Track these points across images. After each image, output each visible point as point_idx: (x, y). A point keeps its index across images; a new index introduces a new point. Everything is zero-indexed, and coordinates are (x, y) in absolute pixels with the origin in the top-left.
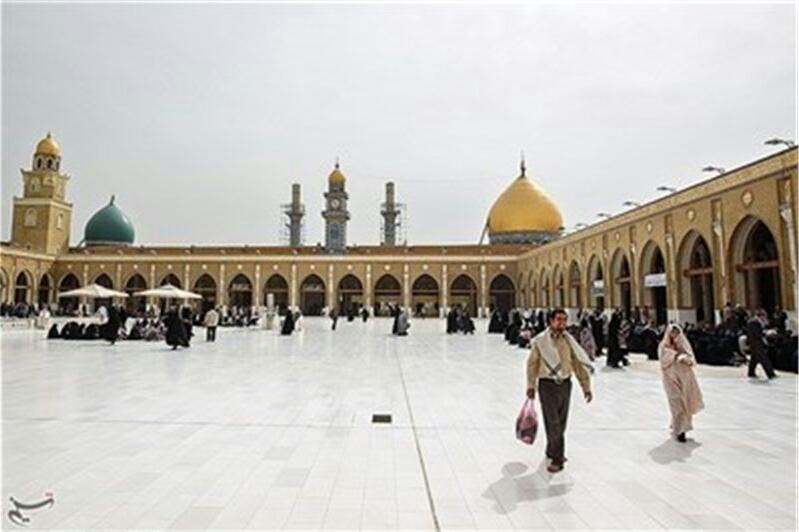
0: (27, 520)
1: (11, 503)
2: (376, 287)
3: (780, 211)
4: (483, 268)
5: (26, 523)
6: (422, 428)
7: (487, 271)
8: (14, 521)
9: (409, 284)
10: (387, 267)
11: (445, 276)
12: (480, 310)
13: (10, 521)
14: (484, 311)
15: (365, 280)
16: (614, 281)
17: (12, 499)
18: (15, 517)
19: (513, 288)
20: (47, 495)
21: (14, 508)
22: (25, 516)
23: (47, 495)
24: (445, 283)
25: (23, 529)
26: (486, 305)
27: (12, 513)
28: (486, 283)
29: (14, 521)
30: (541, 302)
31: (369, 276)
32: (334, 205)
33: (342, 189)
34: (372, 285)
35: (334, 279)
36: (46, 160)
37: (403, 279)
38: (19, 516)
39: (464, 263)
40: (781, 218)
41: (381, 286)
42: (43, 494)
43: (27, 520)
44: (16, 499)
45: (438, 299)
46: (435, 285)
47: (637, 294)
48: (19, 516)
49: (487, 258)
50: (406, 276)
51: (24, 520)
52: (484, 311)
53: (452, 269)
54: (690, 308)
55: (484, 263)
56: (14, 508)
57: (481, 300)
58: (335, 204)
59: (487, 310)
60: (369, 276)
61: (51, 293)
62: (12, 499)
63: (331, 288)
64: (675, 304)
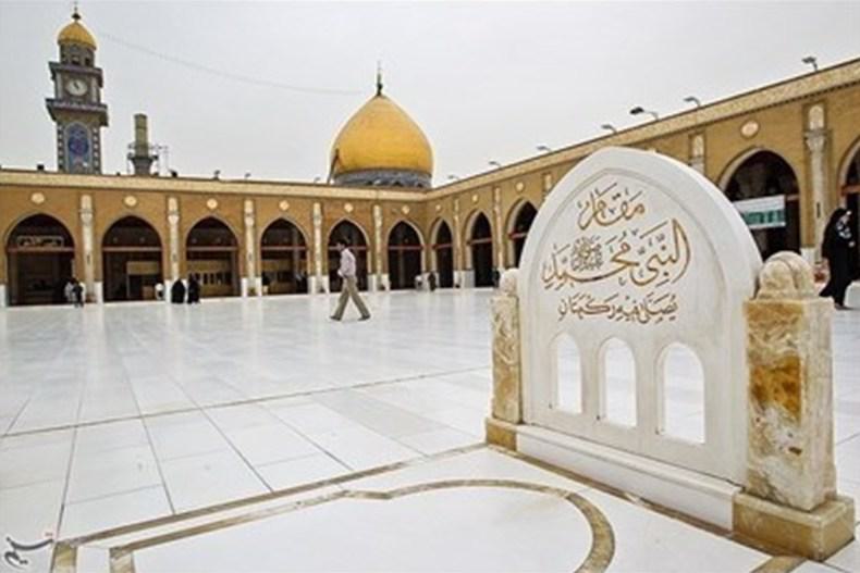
0: (26, 562)
1: (8, 544)
2: (189, 243)
3: (806, 139)
4: (377, 210)
5: (24, 566)
6: (259, 466)
7: (383, 214)
8: (10, 563)
9: (255, 235)
10: (212, 204)
11: (318, 223)
12: (244, 282)
13: (6, 563)
14: (379, 279)
15: (167, 229)
16: (507, 236)
17: (8, 539)
18: (12, 559)
19: (417, 242)
20: (47, 534)
21: (11, 549)
22: (22, 558)
23: (47, 534)
24: (318, 233)
25: (15, 570)
26: (324, 274)
27: (8, 555)
28: (383, 234)
29: (10, 563)
30: (464, 263)
31: (173, 219)
32: (72, 89)
33: (89, 62)
34: (180, 237)
35: (95, 224)
36: (76, 62)
37: (243, 226)
38: (16, 557)
39: (349, 200)
40: (806, 147)
41: (194, 241)
42: (43, 534)
43: (26, 562)
44: (13, 539)
45: (230, 264)
46: (230, 239)
47: (460, 257)
48: (16, 557)
49: (385, 194)
50: (249, 222)
51: (22, 562)
52: (379, 279)
53: (329, 208)
54: (470, 270)
55: (378, 202)
56: (11, 549)
57: (245, 263)
58: (77, 89)
59: (259, 281)
60: (173, 219)
61: (423, 254)
62: (8, 539)
63: (88, 242)
64: (460, 266)
